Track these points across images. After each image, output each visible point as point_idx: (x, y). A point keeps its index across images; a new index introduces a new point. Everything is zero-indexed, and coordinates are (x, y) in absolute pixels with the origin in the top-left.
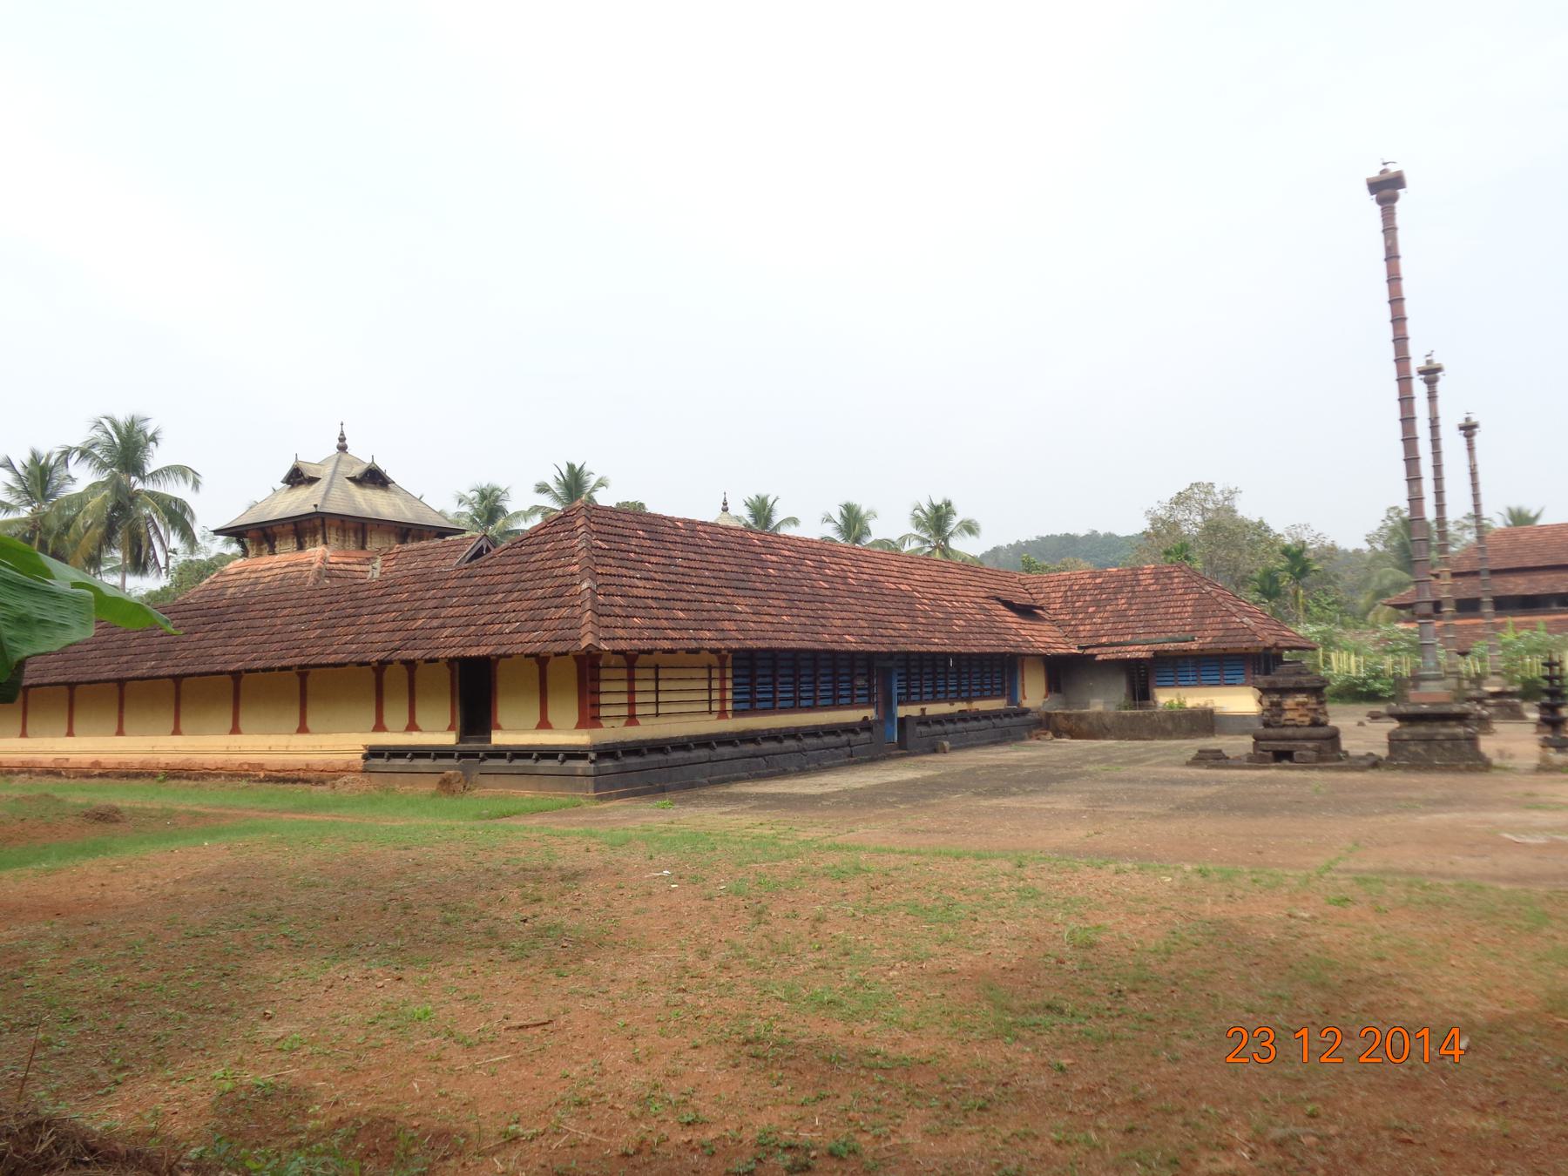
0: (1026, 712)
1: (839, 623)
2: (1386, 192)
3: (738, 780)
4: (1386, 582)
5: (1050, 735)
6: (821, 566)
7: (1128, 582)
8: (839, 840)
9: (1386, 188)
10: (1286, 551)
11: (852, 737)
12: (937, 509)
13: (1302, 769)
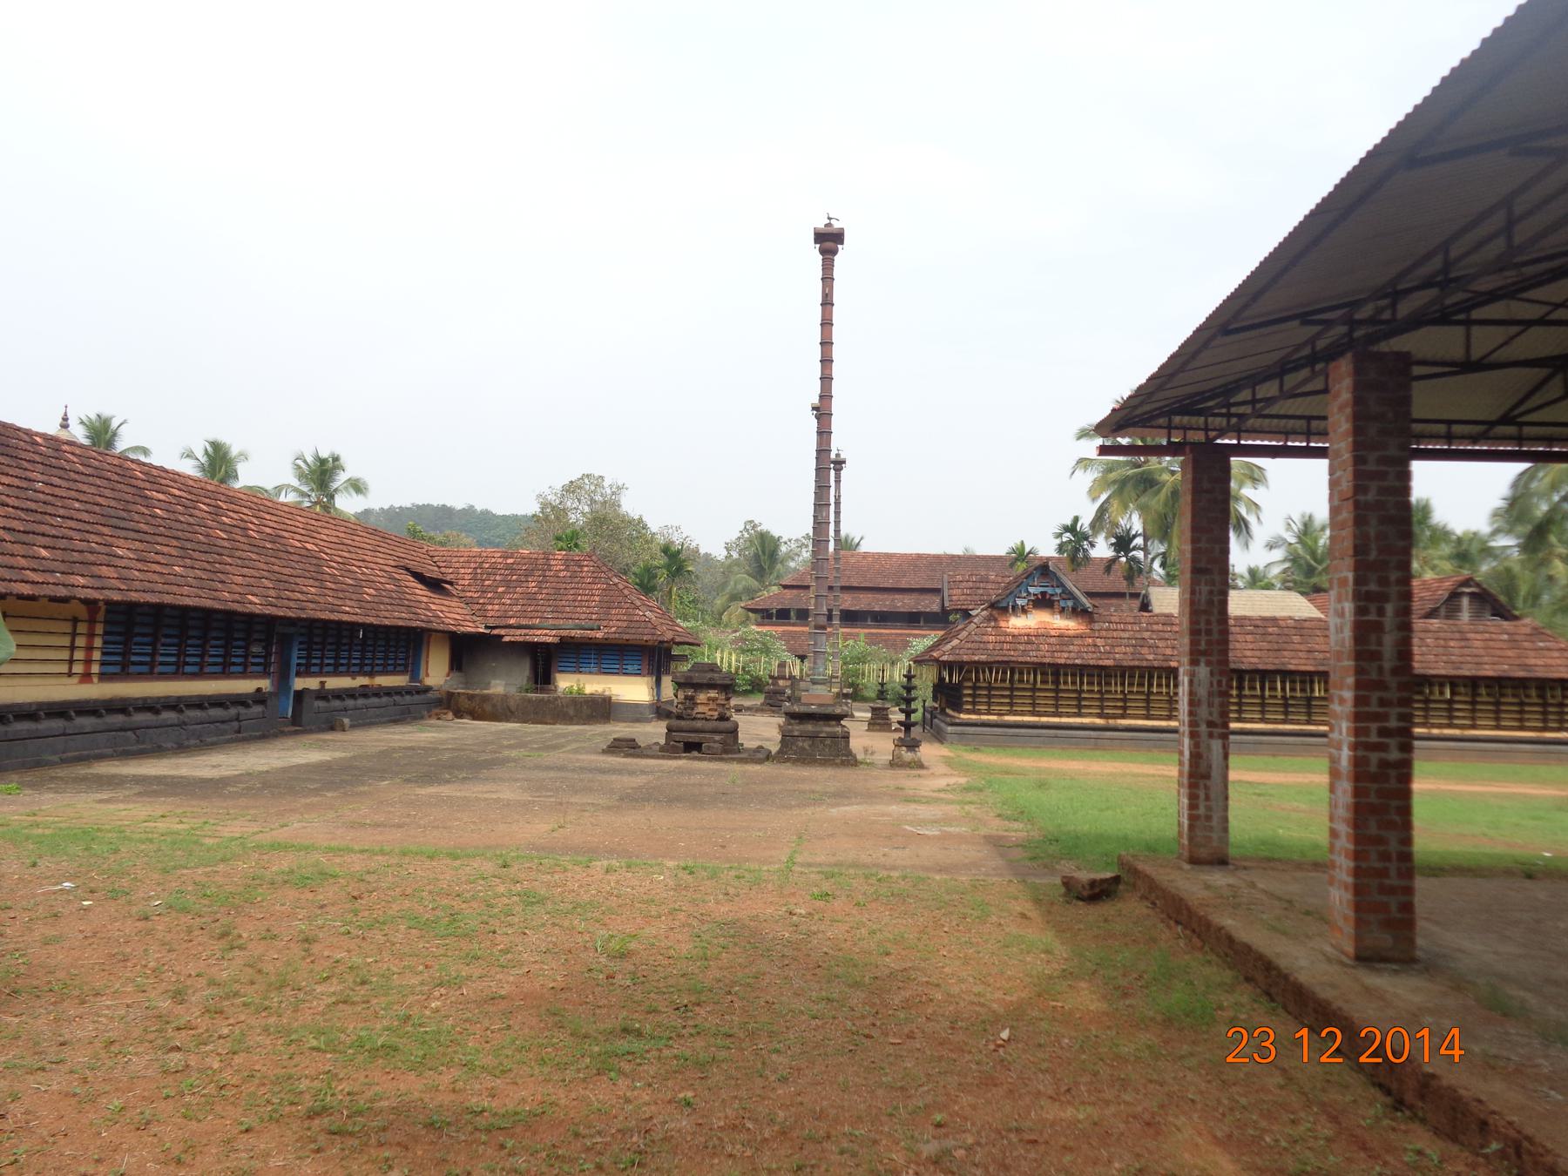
0: (428, 689)
1: (239, 580)
2: (829, 245)
3: (101, 757)
4: (740, 587)
5: (450, 715)
6: (217, 512)
7: (537, 567)
8: (281, 835)
9: (829, 240)
10: (666, 550)
11: (242, 710)
12: (323, 462)
13: (710, 760)
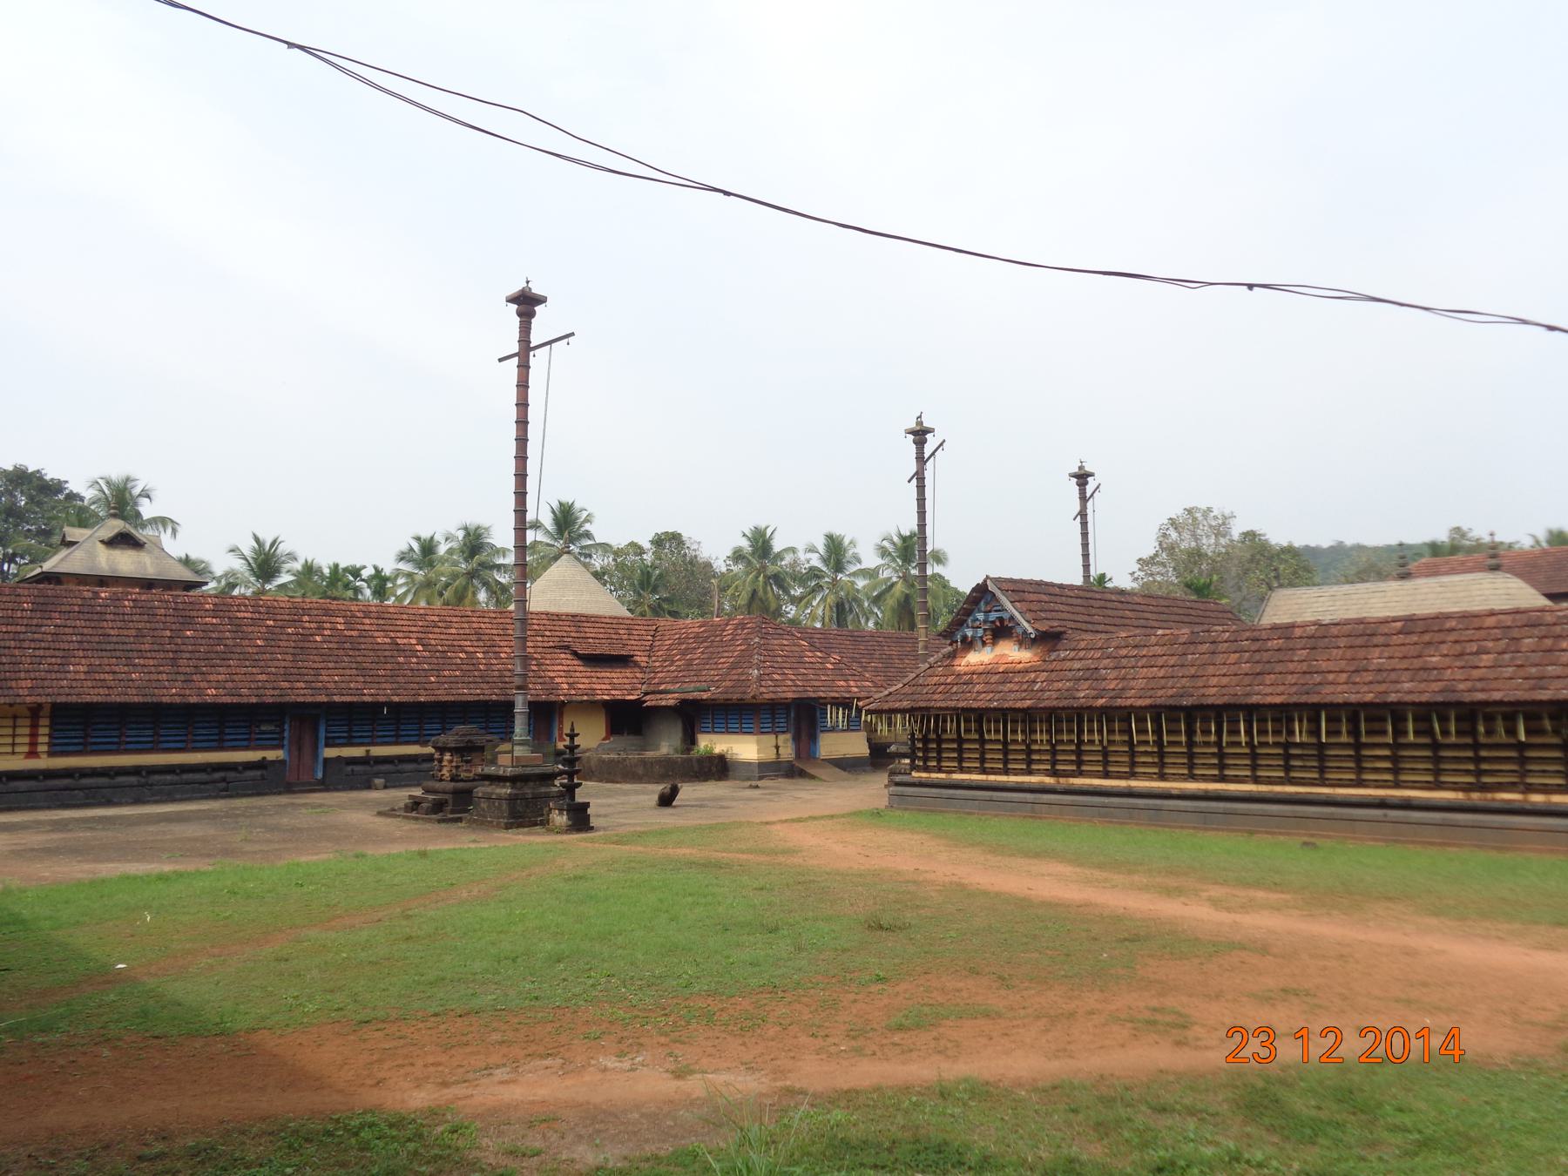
9: (526, 303)
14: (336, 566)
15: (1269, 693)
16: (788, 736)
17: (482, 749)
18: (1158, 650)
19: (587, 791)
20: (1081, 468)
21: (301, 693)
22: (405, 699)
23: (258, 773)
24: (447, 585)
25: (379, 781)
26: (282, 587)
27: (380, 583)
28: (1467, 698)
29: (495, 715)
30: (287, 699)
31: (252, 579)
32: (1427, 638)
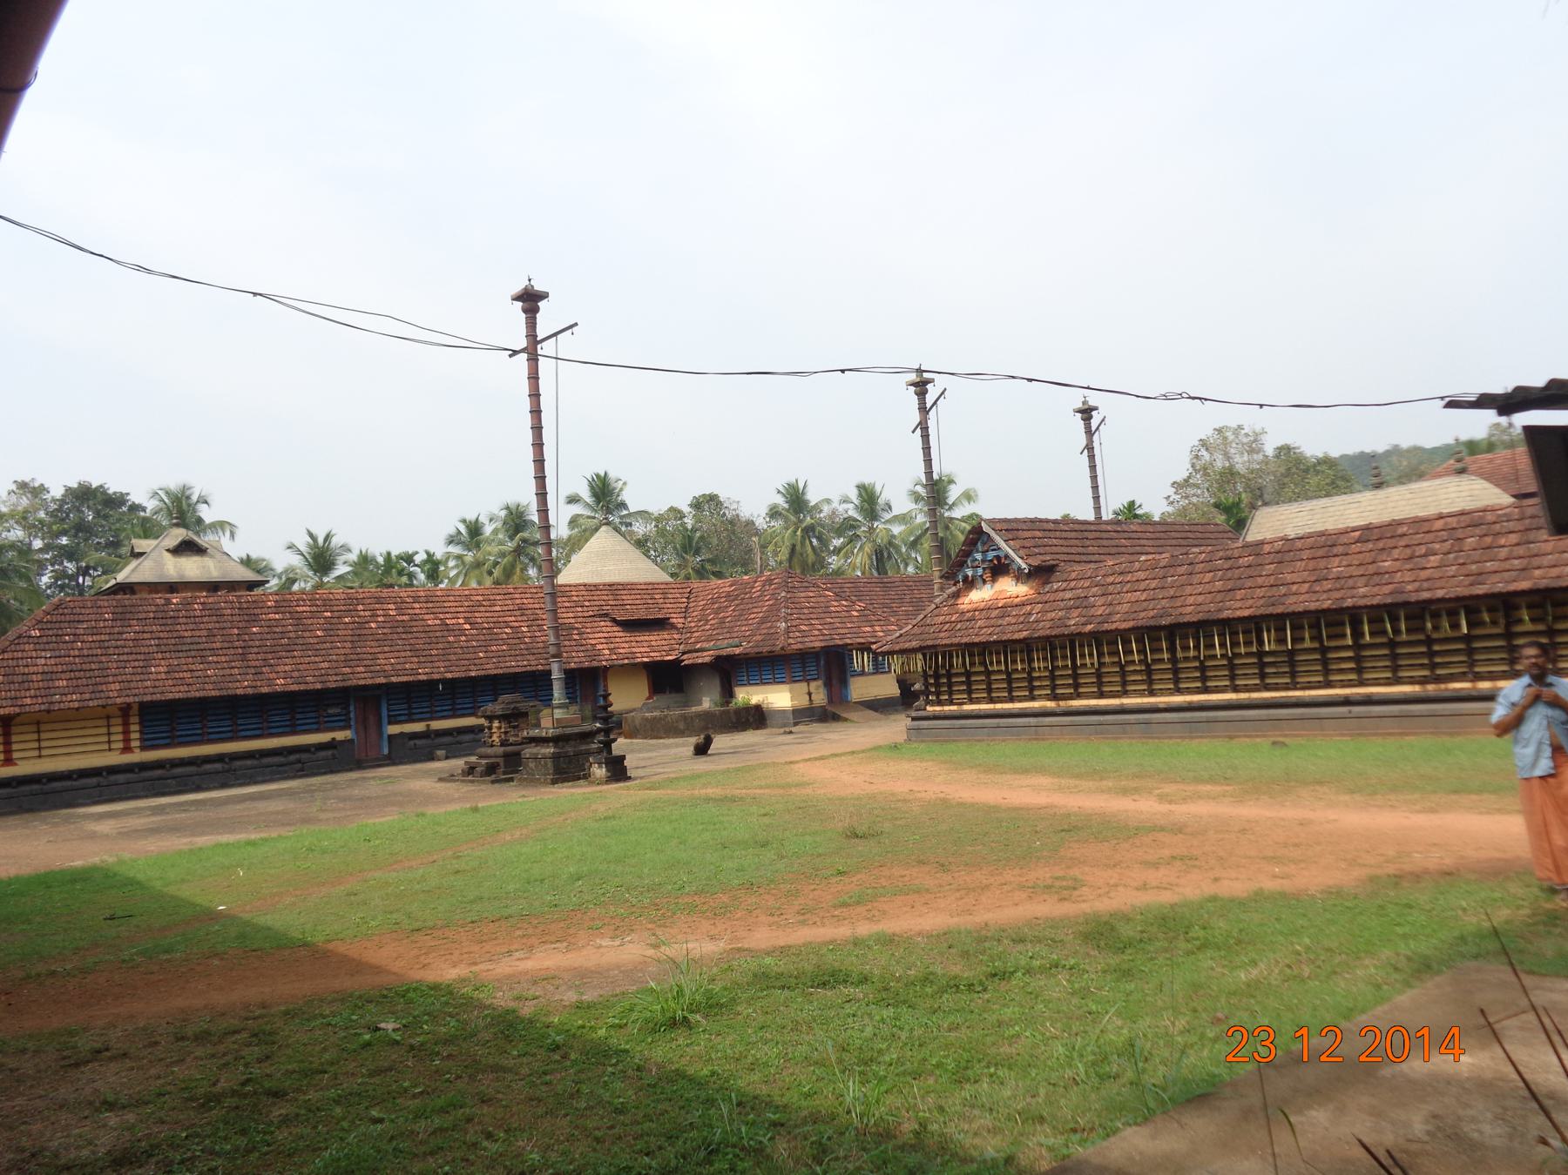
9: (530, 300)
14: (389, 554)
15: (1239, 608)
16: (820, 683)
17: (526, 714)
18: (1142, 575)
19: (620, 745)
20: (1084, 403)
21: (361, 677)
22: (457, 675)
23: (330, 753)
24: (496, 564)
25: (440, 753)
26: (339, 578)
27: (433, 567)
28: (1413, 598)
29: (536, 683)
30: (349, 683)
31: (311, 573)
32: (1381, 544)
